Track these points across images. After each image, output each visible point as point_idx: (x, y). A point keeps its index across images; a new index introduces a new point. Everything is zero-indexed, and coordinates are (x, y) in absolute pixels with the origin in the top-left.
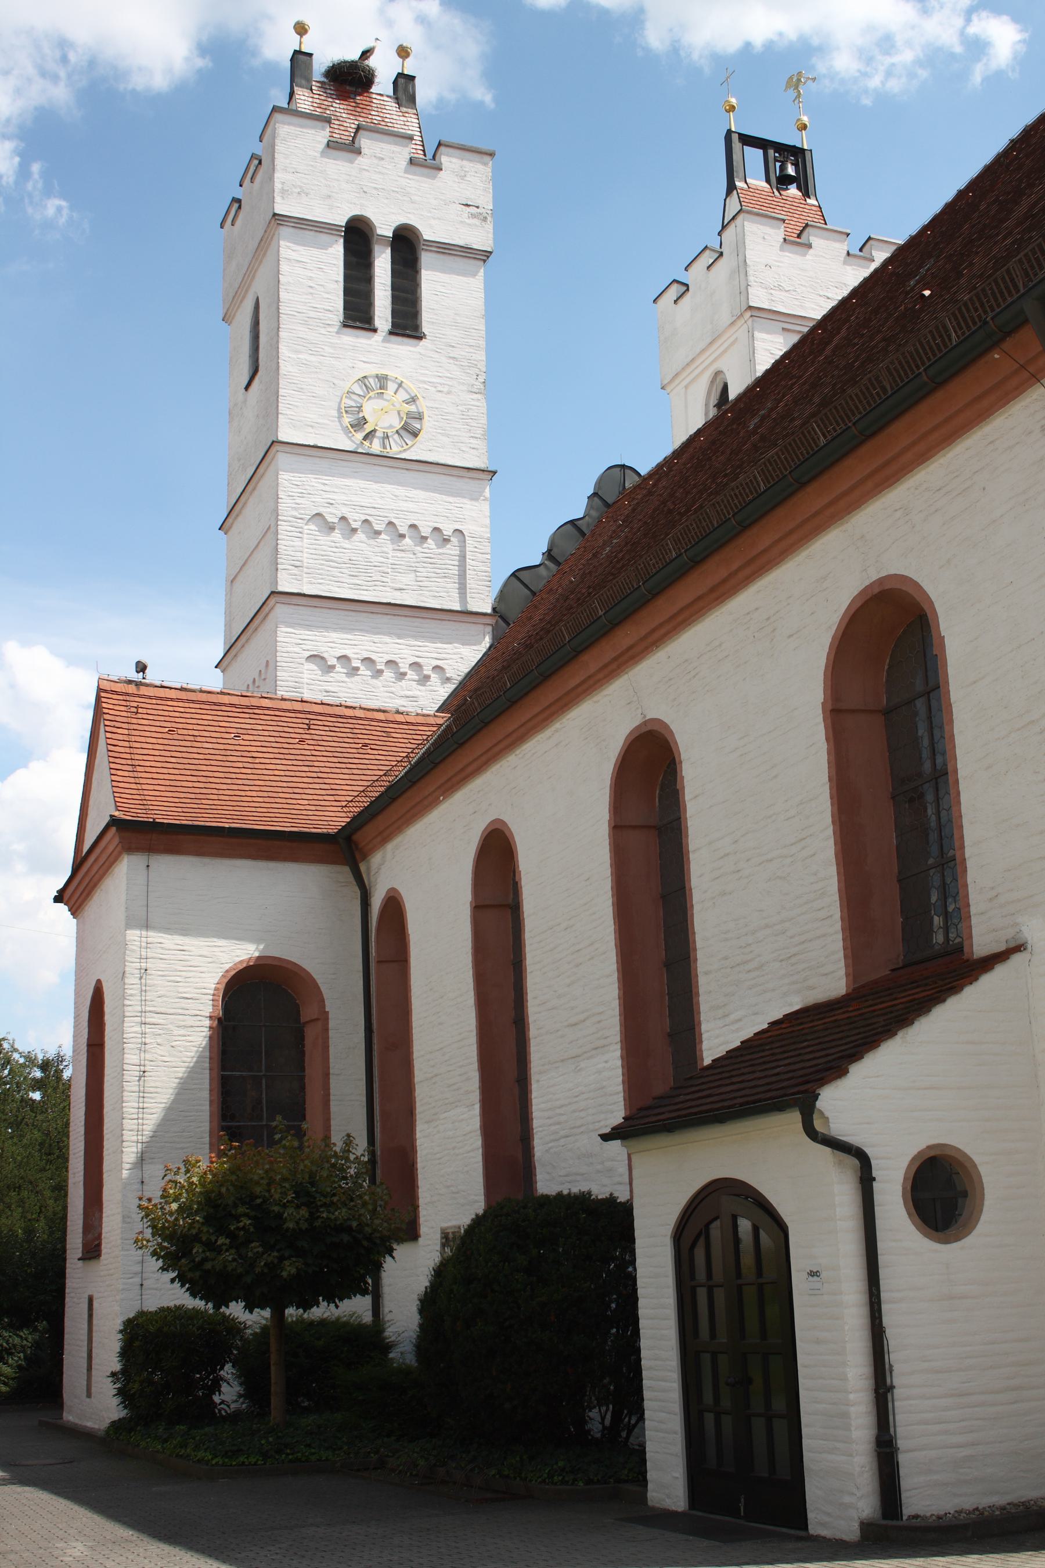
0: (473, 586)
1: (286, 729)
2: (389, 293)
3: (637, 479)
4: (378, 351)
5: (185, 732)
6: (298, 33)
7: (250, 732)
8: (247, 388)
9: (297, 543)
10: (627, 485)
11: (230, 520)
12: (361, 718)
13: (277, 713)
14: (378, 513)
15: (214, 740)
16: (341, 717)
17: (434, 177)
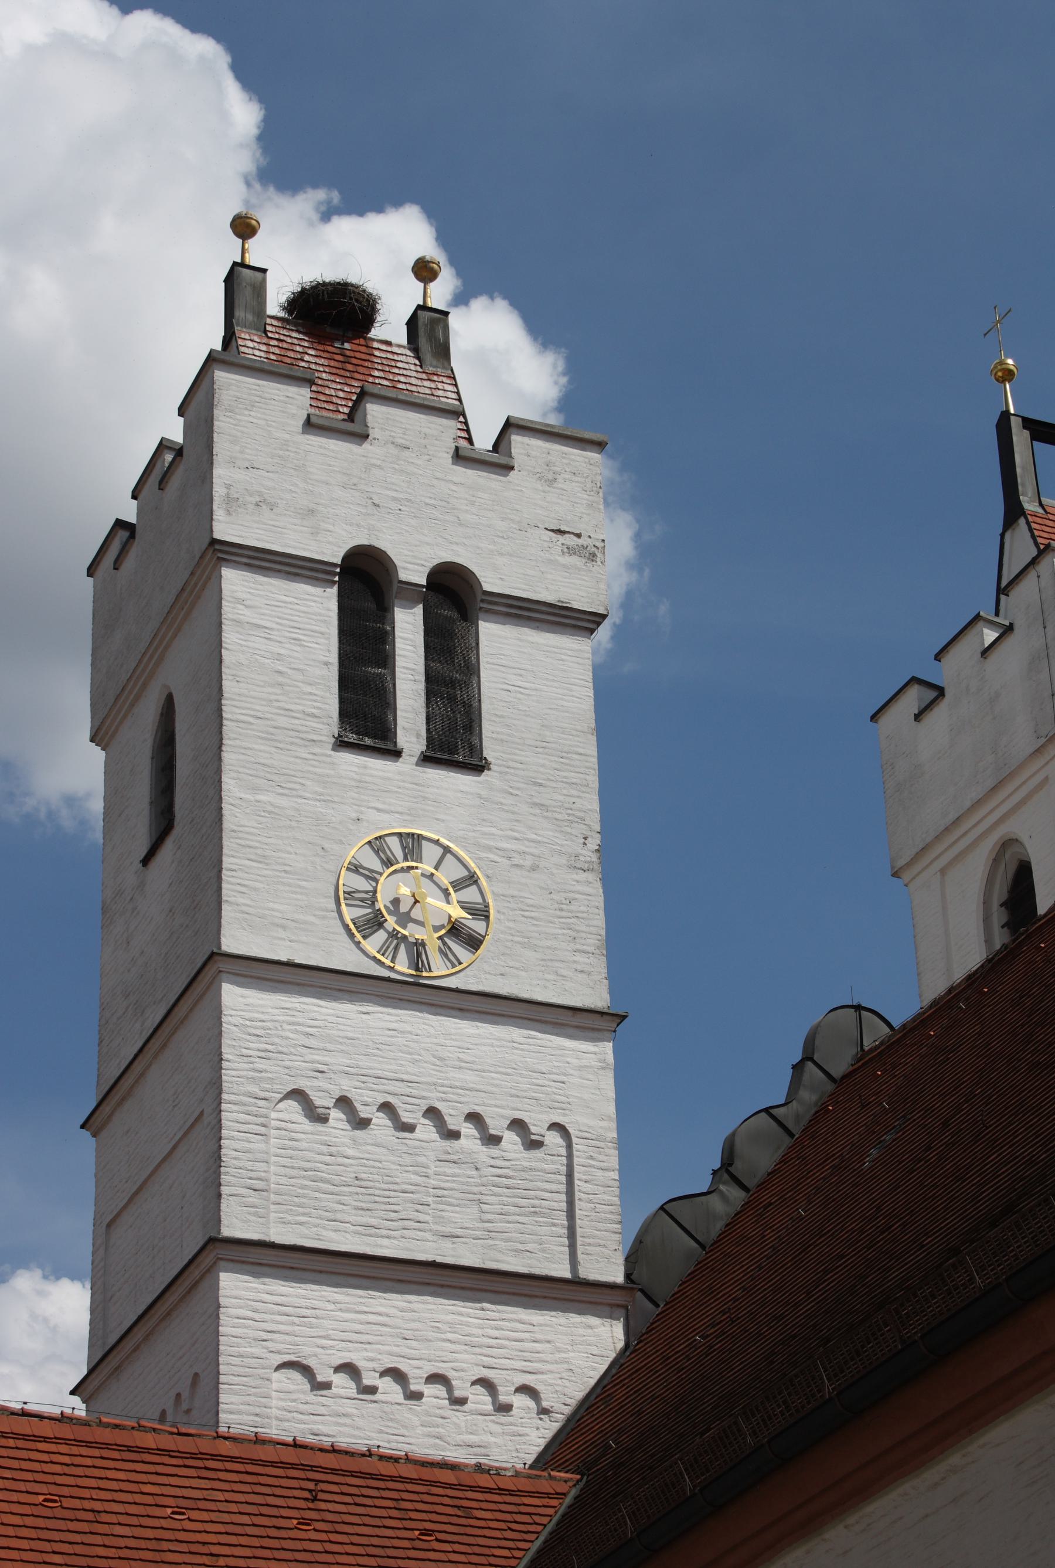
0: (588, 1231)
1: (271, 1500)
2: (421, 686)
3: (887, 1030)
4: (401, 789)
5: (77, 1504)
6: (238, 234)
7: (202, 1505)
8: (146, 861)
9: (258, 1144)
10: (865, 1043)
11: (106, 1109)
12: (411, 1481)
13: (250, 1468)
14: (408, 1091)
15: (134, 1521)
16: (372, 1476)
17: (506, 476)
